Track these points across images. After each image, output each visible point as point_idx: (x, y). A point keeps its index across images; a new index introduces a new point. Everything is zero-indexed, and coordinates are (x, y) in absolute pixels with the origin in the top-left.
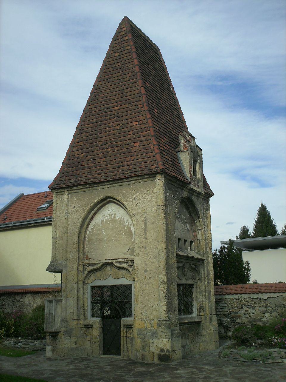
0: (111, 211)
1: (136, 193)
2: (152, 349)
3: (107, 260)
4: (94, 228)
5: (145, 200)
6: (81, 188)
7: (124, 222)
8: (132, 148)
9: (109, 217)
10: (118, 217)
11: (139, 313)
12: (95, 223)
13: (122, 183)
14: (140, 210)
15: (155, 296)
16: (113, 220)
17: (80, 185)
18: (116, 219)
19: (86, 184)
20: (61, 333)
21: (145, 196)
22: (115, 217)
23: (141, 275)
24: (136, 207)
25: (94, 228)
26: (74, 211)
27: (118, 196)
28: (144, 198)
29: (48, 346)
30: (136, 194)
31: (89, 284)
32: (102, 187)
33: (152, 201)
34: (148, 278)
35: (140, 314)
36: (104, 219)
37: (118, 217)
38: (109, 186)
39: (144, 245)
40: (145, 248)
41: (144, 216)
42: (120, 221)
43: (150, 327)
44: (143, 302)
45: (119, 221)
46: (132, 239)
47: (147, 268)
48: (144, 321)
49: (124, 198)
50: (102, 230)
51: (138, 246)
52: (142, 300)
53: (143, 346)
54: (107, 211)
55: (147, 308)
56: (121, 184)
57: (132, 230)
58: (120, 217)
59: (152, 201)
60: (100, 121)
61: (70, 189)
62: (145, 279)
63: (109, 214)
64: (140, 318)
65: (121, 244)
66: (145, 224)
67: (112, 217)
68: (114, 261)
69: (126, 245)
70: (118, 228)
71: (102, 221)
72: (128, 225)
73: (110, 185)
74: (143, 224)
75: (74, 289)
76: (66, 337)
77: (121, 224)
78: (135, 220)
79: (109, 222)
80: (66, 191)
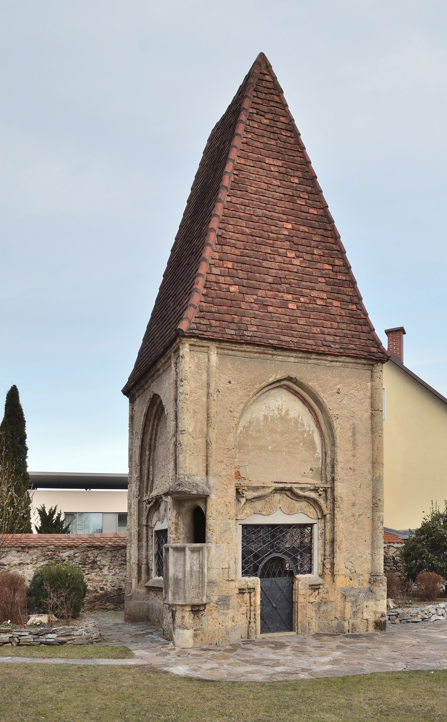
0: (280, 403)
1: (341, 384)
2: (366, 616)
3: (274, 482)
4: (249, 427)
5: (354, 397)
6: (248, 350)
7: (303, 425)
8: (329, 308)
9: (276, 412)
10: (293, 414)
11: (343, 566)
12: (252, 418)
13: (320, 361)
14: (346, 411)
15: (365, 541)
16: (284, 419)
17: (247, 343)
18: (288, 417)
19: (258, 345)
20: (212, 604)
21: (353, 391)
22: (287, 413)
23: (346, 510)
24: (340, 405)
25: (249, 427)
26: (228, 389)
27: (310, 380)
28: (351, 394)
29: (187, 629)
30: (340, 385)
31: (240, 521)
32: (283, 357)
33: (364, 402)
34: (357, 515)
35: (344, 568)
36: (268, 413)
37: (293, 414)
38: (297, 360)
39: (351, 466)
40: (354, 470)
41: (351, 422)
42: (297, 422)
43: (357, 585)
44: (348, 550)
45: (294, 422)
46: (314, 454)
47: (355, 501)
48: (350, 577)
49: (321, 386)
50: (264, 433)
51: (343, 466)
52: (347, 547)
53: (354, 612)
54: (274, 401)
55: (354, 558)
56: (317, 361)
57: (315, 439)
58: (296, 416)
59: (364, 402)
60: (259, 236)
61: (224, 345)
62: (353, 515)
63: (277, 406)
64: (344, 573)
65: (297, 461)
66: (354, 435)
67: (283, 413)
68: (296, 485)
69: (305, 462)
70: (292, 433)
71: (265, 417)
72: (310, 431)
73: (300, 360)
74: (350, 434)
75: (231, 528)
76: (222, 611)
77: (297, 427)
78: (339, 426)
79: (277, 420)
80: (213, 346)
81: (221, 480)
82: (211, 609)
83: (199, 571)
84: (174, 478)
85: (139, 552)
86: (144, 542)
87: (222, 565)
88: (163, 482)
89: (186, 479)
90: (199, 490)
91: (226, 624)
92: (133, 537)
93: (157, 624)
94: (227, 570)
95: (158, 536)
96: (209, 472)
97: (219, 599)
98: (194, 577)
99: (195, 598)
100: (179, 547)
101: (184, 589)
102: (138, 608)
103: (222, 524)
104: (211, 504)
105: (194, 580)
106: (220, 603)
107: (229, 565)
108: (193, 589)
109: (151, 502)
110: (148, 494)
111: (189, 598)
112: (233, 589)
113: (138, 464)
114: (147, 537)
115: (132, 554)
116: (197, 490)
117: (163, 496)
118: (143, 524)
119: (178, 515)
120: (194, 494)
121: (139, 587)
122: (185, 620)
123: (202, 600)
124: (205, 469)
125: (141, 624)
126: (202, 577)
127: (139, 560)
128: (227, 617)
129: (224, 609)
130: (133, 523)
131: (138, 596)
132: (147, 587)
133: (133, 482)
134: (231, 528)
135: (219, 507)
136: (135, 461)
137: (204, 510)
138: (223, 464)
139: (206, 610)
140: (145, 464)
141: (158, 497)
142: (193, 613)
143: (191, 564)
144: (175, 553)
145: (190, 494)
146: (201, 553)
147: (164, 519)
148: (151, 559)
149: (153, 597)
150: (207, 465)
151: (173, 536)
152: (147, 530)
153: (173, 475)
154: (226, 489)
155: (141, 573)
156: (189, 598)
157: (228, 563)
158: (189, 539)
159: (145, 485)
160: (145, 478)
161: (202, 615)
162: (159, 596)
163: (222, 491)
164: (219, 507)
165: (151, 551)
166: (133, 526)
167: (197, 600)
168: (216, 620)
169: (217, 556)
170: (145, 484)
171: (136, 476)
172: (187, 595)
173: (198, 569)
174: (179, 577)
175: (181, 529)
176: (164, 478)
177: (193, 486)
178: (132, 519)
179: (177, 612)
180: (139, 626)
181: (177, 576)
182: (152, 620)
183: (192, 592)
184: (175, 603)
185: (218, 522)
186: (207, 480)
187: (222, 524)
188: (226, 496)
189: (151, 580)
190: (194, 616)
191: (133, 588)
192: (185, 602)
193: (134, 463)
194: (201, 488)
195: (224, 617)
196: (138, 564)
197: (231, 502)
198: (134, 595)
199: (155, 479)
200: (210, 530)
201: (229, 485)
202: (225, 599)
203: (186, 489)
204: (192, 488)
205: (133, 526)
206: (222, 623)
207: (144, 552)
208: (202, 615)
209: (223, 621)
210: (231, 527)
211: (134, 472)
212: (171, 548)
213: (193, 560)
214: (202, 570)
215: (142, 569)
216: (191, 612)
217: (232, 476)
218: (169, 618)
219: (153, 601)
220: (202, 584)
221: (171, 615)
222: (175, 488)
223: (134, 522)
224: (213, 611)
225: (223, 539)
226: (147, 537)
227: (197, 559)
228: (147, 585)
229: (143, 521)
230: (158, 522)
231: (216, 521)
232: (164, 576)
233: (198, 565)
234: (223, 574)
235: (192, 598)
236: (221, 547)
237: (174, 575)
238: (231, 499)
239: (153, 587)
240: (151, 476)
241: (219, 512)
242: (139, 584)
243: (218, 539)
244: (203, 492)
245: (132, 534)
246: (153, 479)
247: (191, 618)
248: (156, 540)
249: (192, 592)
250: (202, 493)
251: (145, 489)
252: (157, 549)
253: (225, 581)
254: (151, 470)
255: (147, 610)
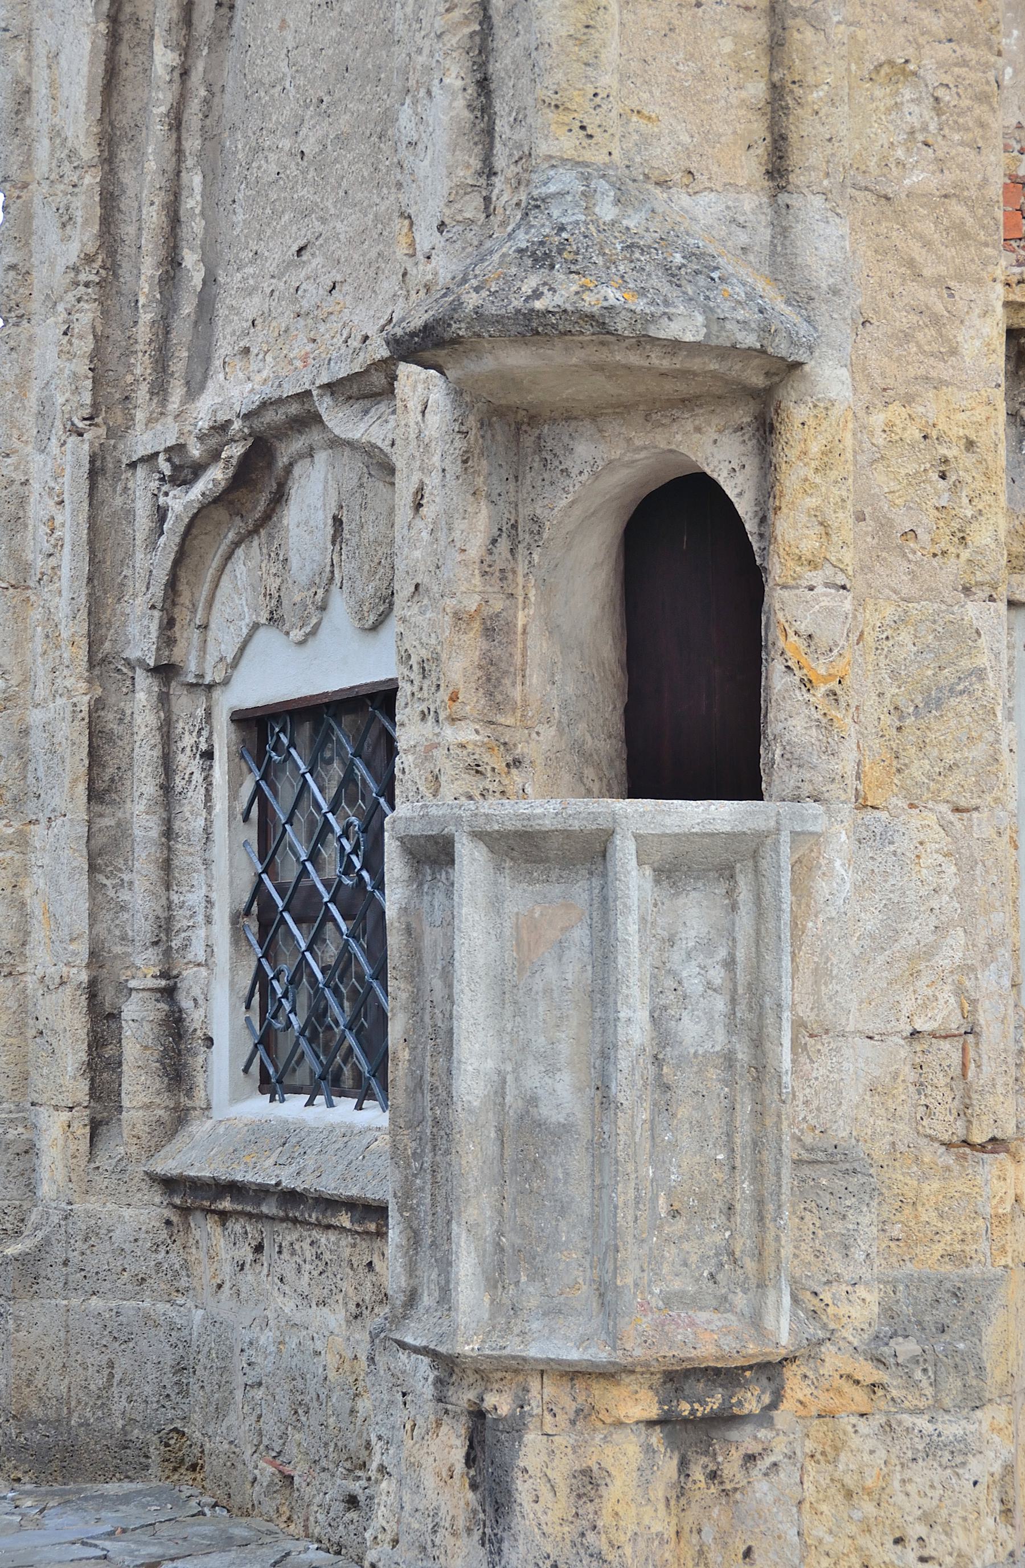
75: (979, 673)
76: (922, 1422)
81: (897, 237)
82: (825, 1400)
83: (729, 1059)
84: (471, 207)
85: (95, 888)
86: (139, 807)
87: (908, 1006)
88: (312, 294)
89: (606, 211)
90: (724, 309)
91: (961, 1541)
92: (40, 765)
93: (268, 1506)
94: (950, 1051)
95: (260, 757)
96: (795, 158)
97: (889, 1313)
98: (683, 1112)
99: (693, 1302)
100: (545, 835)
101: (595, 1221)
102: (95, 1357)
103: (905, 636)
104: (815, 448)
105: (686, 1140)
106: (907, 1348)
107: (968, 1005)
108: (679, 1225)
109: (198, 470)
110: (175, 402)
111: (645, 1308)
112: (1000, 1219)
113: (88, 152)
114: (167, 764)
115: (36, 906)
116: (707, 311)
117: (324, 406)
118: (133, 653)
119: (504, 544)
120: (675, 346)
121: (101, 1182)
122: (608, 1507)
123: (756, 1320)
124: (759, 128)
125: (125, 1499)
126: (759, 1115)
127: (96, 956)
128: (968, 1476)
129: (937, 1405)
130: (39, 644)
131: (92, 1263)
132: (169, 1184)
133: (36, 305)
134: (979, 673)
135: (881, 480)
136: (55, 133)
137: (744, 507)
138: (907, 93)
139: (782, 1416)
140: (140, 151)
141: (270, 417)
142: (672, 1443)
143: (656, 991)
144: (505, 881)
145: (643, 341)
146: (744, 894)
147: (323, 608)
148: (196, 950)
149: (228, 1269)
150: (777, 90)
151: (467, 734)
152: (164, 700)
153: (465, 189)
154: (936, 321)
155: (116, 1064)
156: (645, 1308)
157: (960, 991)
158: (589, 772)
159: (143, 333)
160: (149, 268)
161: (750, 1458)
162: (286, 1266)
163: (907, 337)
164: (881, 480)
165: (198, 879)
166: (41, 673)
167: (717, 1320)
168: (868, 1508)
169: (871, 922)
170: (146, 317)
171: (73, 252)
172: (627, 1279)
173: (720, 1036)
174: (546, 1111)
175: (535, 678)
176: (315, 261)
177: (672, 274)
178: (36, 614)
179: (531, 1437)
180: (110, 1518)
181: (533, 1101)
182: (213, 1465)
183: (670, 1253)
184: (514, 1347)
185: (870, 617)
186: (781, 231)
187: (905, 636)
188: (939, 384)
189: (199, 1128)
190: (684, 1464)
191: (46, 1189)
192: (614, 1339)
193: (43, 150)
194: (740, 292)
195: (938, 1475)
196: (92, 991)
197: (983, 439)
198: (58, 1252)
199: (230, 280)
200: (807, 684)
201: (964, 291)
202: (940, 1314)
203: (612, 295)
204: (666, 289)
205: (41, 673)
206: (921, 1530)
207: (140, 885)
208: (750, 1458)
209: (928, 1519)
210: (984, 660)
211: (45, 221)
212: (478, 835)
213: (676, 956)
214: (758, 1043)
215: (128, 1030)
216: (656, 1437)
217: (991, 203)
218: (430, 1481)
219: (224, 1306)
220: (757, 1178)
221: (458, 1455)
222: (509, 281)
223: (52, 638)
224: (846, 1422)
225: (919, 769)
226: (167, 764)
227: (706, 946)
228: (168, 1164)
229: (134, 630)
230: (263, 636)
231: (860, 603)
232: (398, 1095)
233: (720, 1004)
234: (920, 1086)
235: (668, 1300)
236: (903, 844)
237: (501, 1091)
238: (980, 413)
239: (234, 1189)
240: (190, 258)
241: (884, 525)
242: (103, 1161)
243: (873, 772)
244: (765, 330)
245: (37, 741)
246: (210, 280)
247: (659, 1491)
248: (247, 788)
249: (670, 1253)
250: (750, 340)
251: (142, 366)
252: (249, 866)
253: (932, 1154)
254: (192, 202)
255: (168, 1380)
